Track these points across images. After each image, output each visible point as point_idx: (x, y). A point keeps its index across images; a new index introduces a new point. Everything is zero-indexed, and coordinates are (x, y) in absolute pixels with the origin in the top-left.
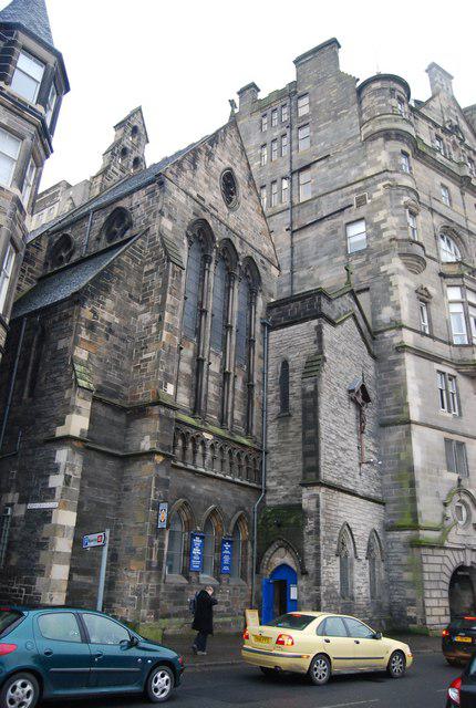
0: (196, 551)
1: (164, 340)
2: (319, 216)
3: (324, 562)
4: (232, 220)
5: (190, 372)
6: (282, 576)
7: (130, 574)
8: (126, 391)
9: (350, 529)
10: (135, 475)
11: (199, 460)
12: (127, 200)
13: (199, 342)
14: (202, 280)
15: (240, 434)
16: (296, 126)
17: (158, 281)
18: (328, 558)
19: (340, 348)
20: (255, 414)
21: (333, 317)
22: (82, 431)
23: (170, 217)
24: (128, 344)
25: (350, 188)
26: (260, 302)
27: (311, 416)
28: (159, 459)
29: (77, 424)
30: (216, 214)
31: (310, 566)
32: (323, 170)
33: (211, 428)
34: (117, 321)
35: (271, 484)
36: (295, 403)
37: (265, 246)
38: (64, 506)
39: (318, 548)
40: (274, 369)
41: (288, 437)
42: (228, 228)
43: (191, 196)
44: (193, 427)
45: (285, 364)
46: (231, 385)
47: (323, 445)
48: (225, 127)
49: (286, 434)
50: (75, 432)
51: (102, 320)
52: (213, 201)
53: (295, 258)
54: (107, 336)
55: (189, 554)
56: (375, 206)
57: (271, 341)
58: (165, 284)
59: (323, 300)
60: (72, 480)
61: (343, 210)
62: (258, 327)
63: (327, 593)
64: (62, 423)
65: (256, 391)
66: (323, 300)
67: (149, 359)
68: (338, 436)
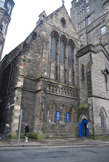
0: (58, 116)
1: (43, 61)
2: (93, 27)
3: (95, 118)
4: (65, 30)
5: (54, 70)
6: (84, 122)
7: (36, 121)
8: (35, 76)
9: (104, 108)
10: (37, 96)
11: (58, 92)
12: (36, 30)
13: (56, 62)
14: (56, 46)
15: (71, 85)
16: (85, 6)
17: (41, 47)
18: (96, 116)
19: (98, 60)
20: (75, 80)
21: (95, 51)
22: (21, 86)
23: (45, 31)
24: (35, 64)
25: (100, 18)
26: (75, 51)
27: (89, 78)
28: (42, 92)
29: (20, 84)
30: (59, 29)
31: (91, 119)
32: (93, 16)
33: (61, 84)
34: (32, 58)
35: (81, 98)
36: (85, 76)
37: (76, 36)
38: (17, 105)
39: (93, 114)
40: (80, 67)
41: (84, 85)
42: (63, 32)
43: (51, 25)
44: (56, 84)
45: (83, 66)
46: (67, 73)
47: (93, 86)
48: (61, 8)
49: (84, 84)
50: (20, 86)
51: (27, 58)
52: (58, 26)
53: (88, 40)
54: (29, 62)
55: (56, 117)
56: (108, 21)
57: (79, 61)
58: (43, 47)
59: (91, 47)
60: (19, 98)
61: (99, 24)
62: (75, 57)
63: (96, 126)
64: (16, 84)
65: (75, 74)
66: (91, 47)
67: (40, 67)
68: (98, 83)
